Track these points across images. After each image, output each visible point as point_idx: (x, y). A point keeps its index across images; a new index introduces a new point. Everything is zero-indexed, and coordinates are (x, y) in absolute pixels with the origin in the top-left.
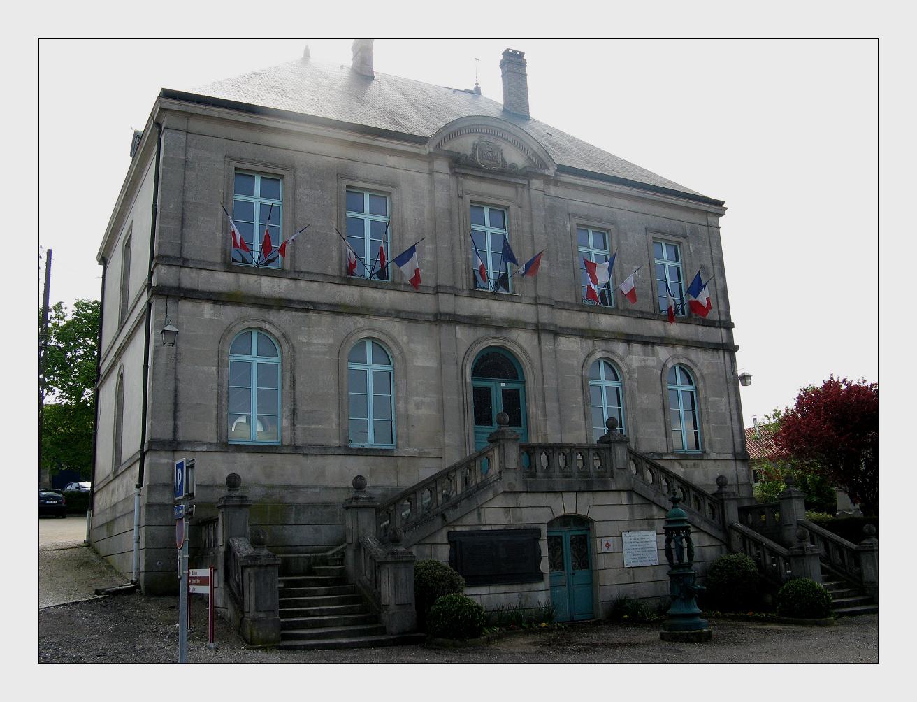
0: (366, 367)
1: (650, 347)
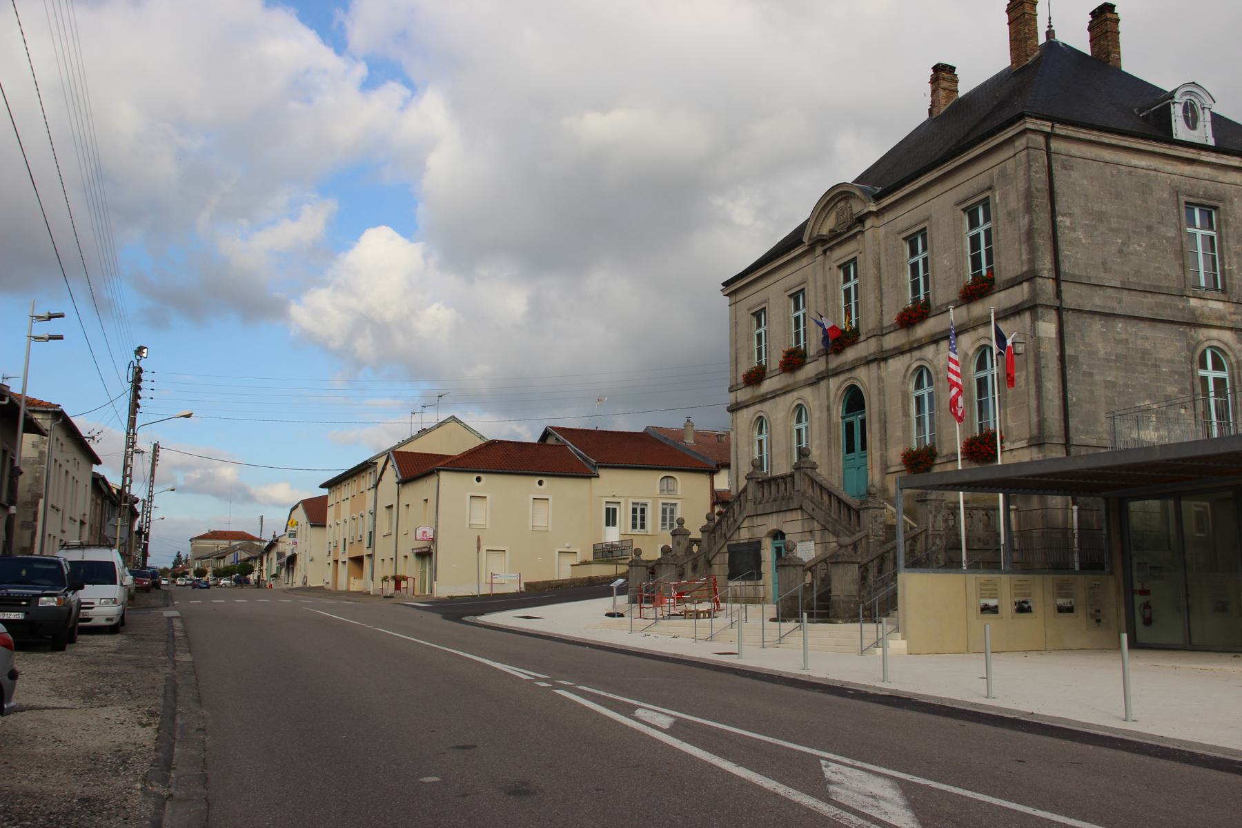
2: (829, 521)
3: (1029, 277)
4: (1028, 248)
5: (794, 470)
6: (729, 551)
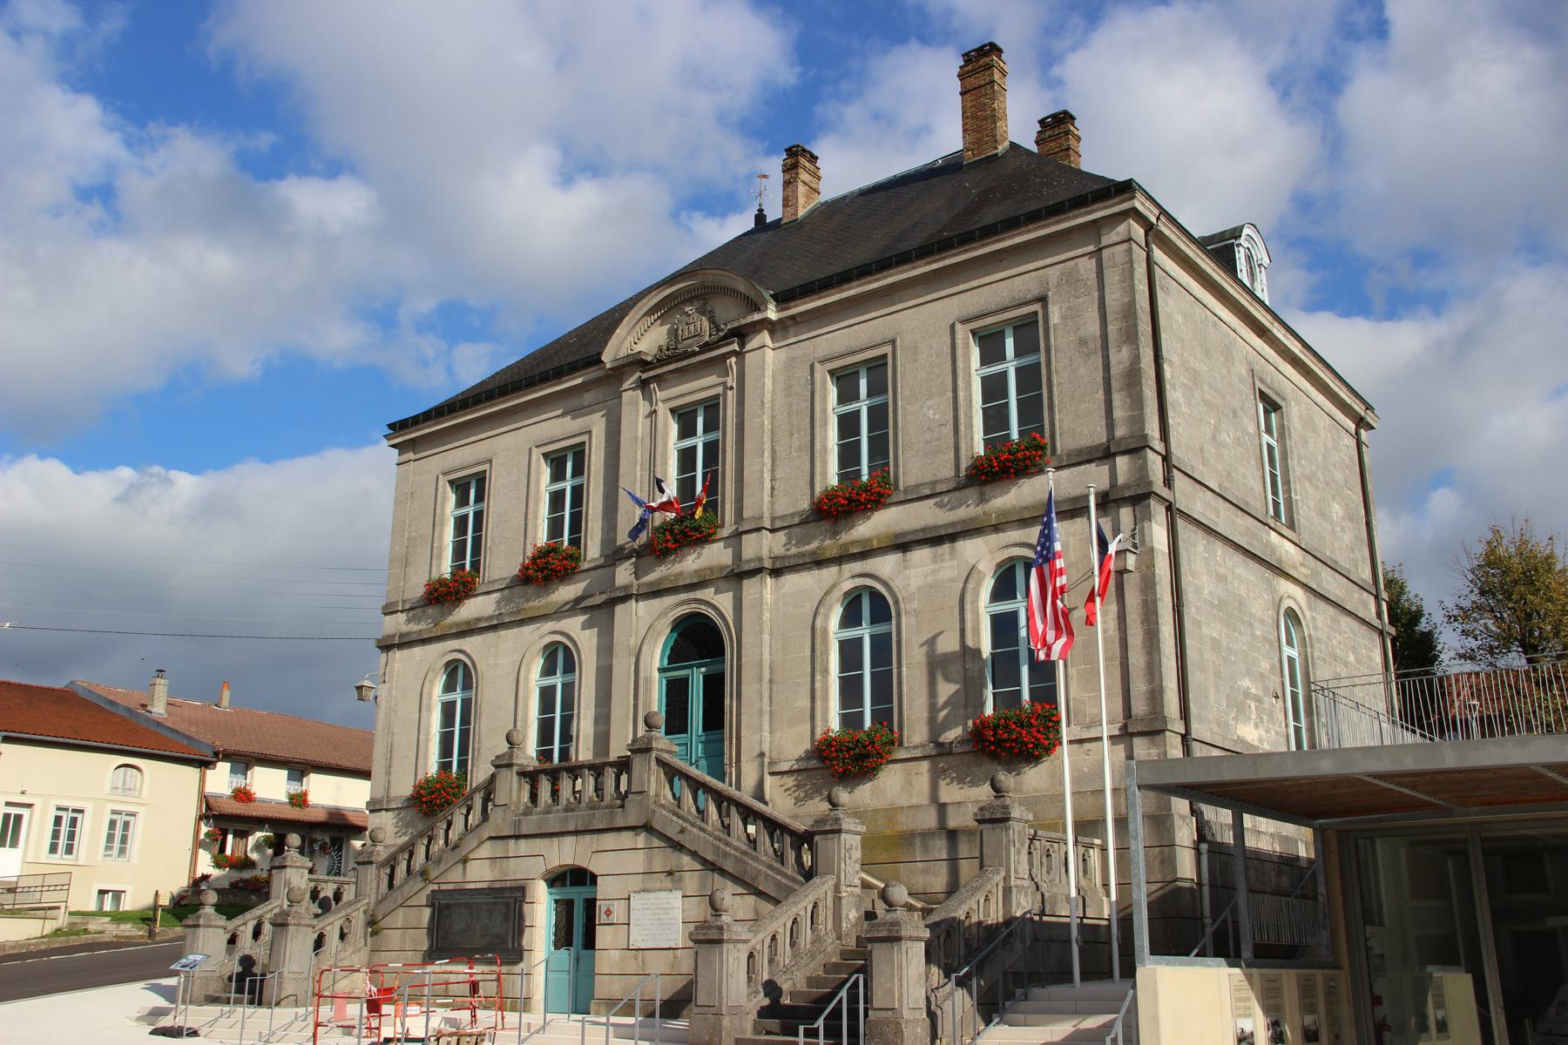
0: (1016, 605)
1: (946, 546)
2: (726, 854)
3: (1134, 446)
4: (1128, 400)
5: (629, 753)
6: (431, 904)
